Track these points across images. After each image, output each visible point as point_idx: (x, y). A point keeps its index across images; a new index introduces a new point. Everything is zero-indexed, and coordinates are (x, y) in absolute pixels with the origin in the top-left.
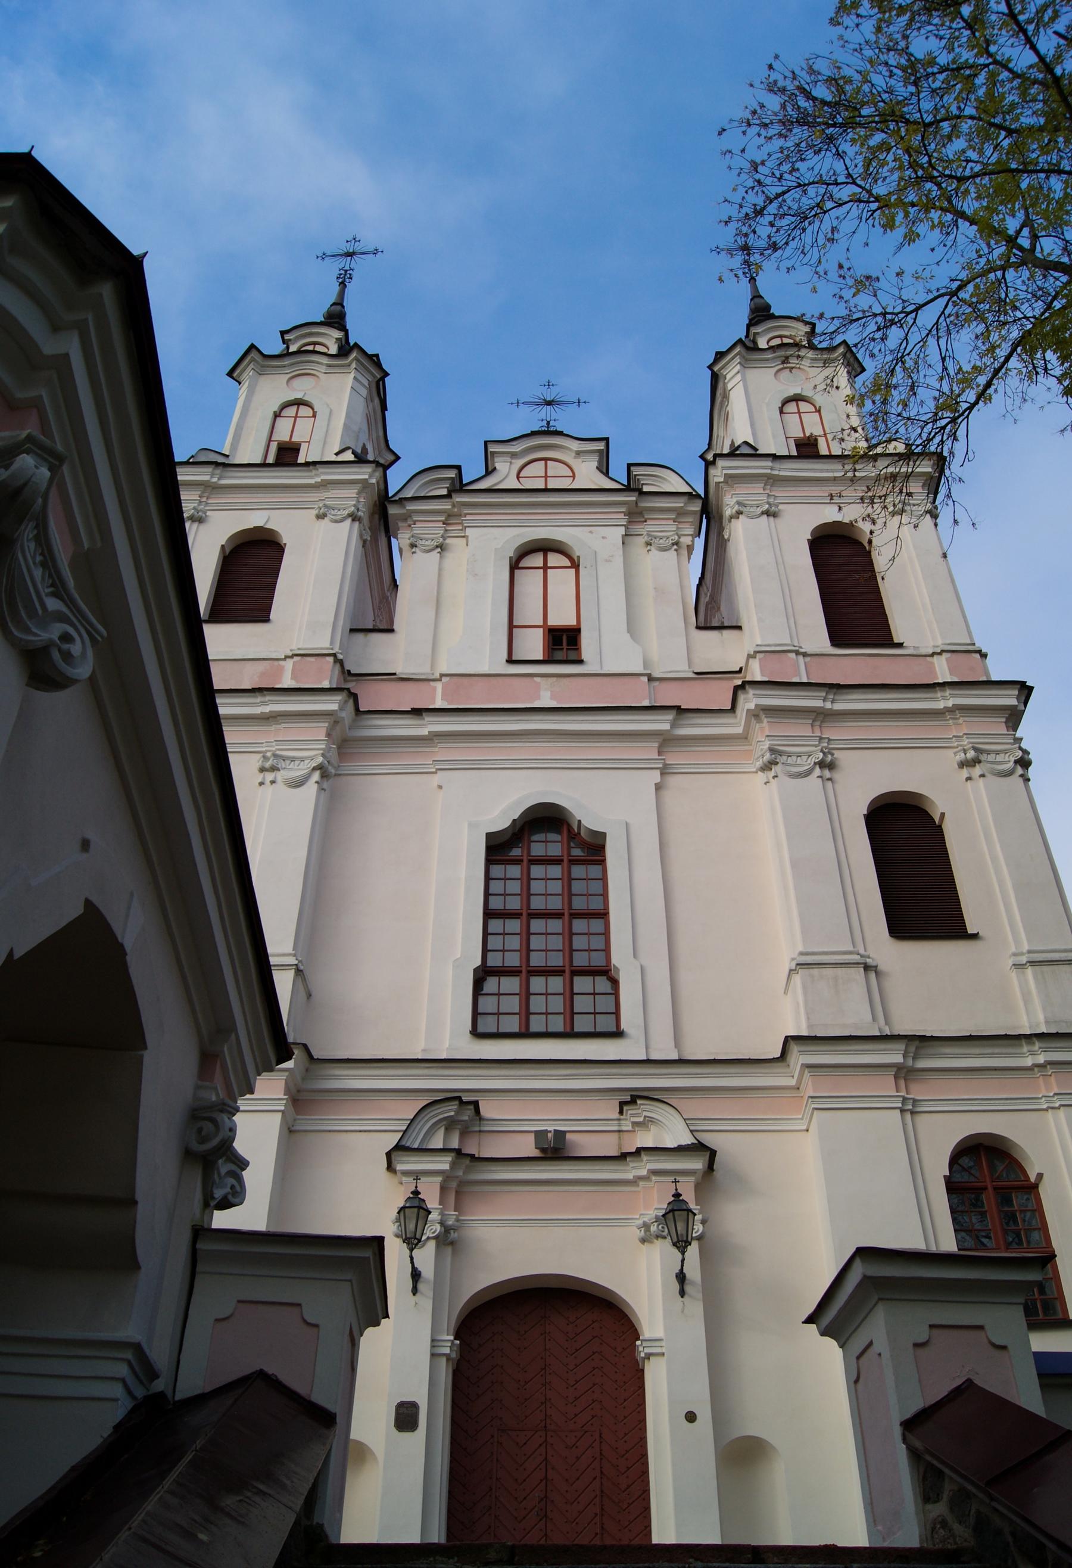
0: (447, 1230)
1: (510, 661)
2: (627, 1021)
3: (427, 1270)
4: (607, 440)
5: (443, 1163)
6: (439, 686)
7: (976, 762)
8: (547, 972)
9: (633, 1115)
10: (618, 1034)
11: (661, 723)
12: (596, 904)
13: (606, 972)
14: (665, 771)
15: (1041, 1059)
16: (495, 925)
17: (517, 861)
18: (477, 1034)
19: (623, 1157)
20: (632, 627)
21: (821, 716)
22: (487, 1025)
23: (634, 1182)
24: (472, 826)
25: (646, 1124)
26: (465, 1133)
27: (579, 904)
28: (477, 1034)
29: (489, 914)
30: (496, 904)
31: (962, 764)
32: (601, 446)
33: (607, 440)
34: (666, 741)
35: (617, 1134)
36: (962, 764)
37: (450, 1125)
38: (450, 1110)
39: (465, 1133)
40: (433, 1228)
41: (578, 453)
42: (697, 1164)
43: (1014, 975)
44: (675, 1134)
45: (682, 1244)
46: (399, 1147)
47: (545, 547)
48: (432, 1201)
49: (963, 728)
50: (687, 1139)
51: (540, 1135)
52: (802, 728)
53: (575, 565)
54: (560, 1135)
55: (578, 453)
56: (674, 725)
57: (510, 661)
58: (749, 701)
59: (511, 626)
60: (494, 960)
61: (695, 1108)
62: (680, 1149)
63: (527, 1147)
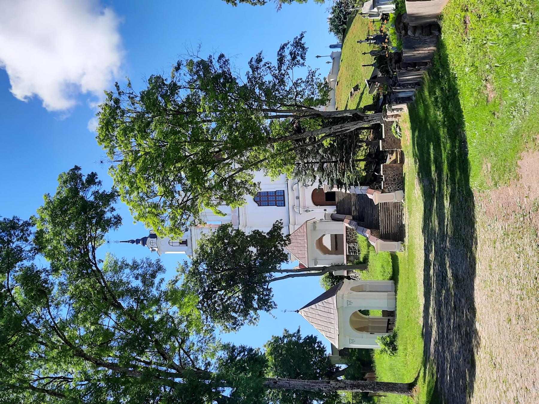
18: (284, 206)
22: (283, 205)
28: (284, 206)
29: (268, 205)
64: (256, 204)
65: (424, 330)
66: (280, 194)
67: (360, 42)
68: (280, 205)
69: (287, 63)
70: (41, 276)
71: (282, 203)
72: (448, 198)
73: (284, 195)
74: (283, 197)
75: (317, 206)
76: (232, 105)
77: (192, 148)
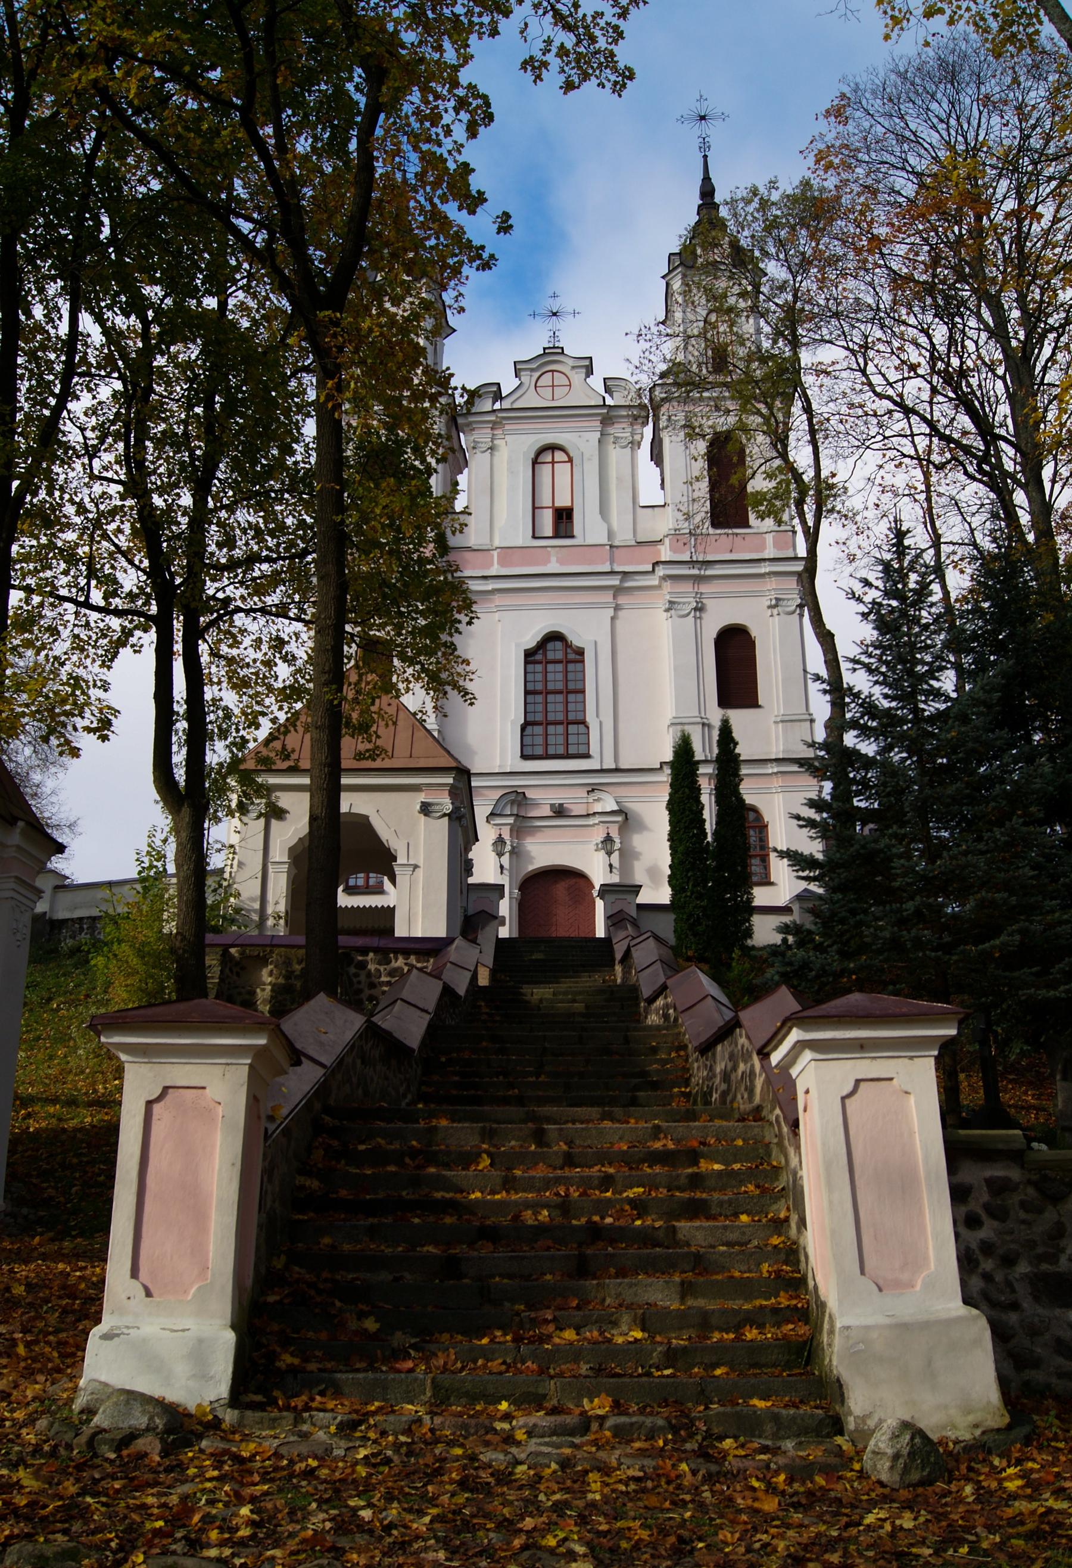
0: (513, 848)
1: (534, 537)
2: (594, 749)
3: (506, 865)
4: (591, 358)
5: (511, 820)
6: (495, 553)
7: (776, 606)
8: (556, 723)
9: (597, 795)
10: (587, 756)
11: (615, 581)
12: (579, 686)
13: (583, 722)
14: (617, 608)
15: (775, 770)
16: (530, 698)
17: (540, 662)
18: (524, 757)
19: (588, 815)
20: (604, 510)
21: (698, 579)
22: (528, 751)
23: (593, 825)
24: (517, 645)
25: (599, 800)
26: (519, 805)
27: (571, 686)
28: (524, 757)
29: (527, 693)
30: (530, 687)
31: (770, 607)
32: (587, 363)
33: (591, 358)
34: (618, 591)
35: (623, 766)
36: (770, 607)
37: (513, 802)
38: (513, 797)
39: (519, 805)
40: (508, 848)
41: (573, 368)
42: (619, 819)
43: (773, 726)
44: (611, 806)
45: (609, 853)
46: (492, 814)
47: (553, 448)
48: (506, 836)
49: (772, 583)
50: (615, 808)
51: (552, 805)
52: (687, 587)
53: (570, 460)
54: (561, 805)
55: (573, 368)
56: (621, 581)
57: (534, 537)
58: (661, 571)
59: (534, 508)
60: (530, 718)
61: (622, 791)
62: (613, 813)
63: (547, 811)
64: (532, 644)
66: (572, 739)
67: (887, 37)
68: (528, 740)
71: (557, 535)
73: (567, 756)
74: (561, 750)
77: (132, 44)
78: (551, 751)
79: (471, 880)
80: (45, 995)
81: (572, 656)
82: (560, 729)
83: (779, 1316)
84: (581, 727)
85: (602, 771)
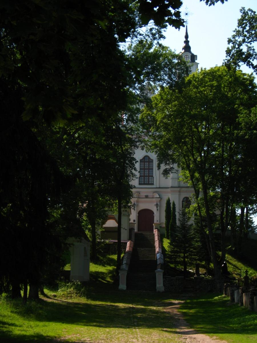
10: (153, 184)
13: (152, 176)
22: (140, 183)
28: (140, 184)
30: (141, 168)
64: (141, 158)
65: (97, 320)
66: (150, 180)
69: (250, 317)
70: (251, 296)
72: (170, 300)
73: (149, 184)
74: (147, 183)
75: (138, 214)
76: (201, 125)
78: (145, 183)
79: (254, 66)
80: (66, 328)
81: (150, 161)
82: (147, 178)
83: (154, 254)
84: (152, 178)
85: (156, 188)
